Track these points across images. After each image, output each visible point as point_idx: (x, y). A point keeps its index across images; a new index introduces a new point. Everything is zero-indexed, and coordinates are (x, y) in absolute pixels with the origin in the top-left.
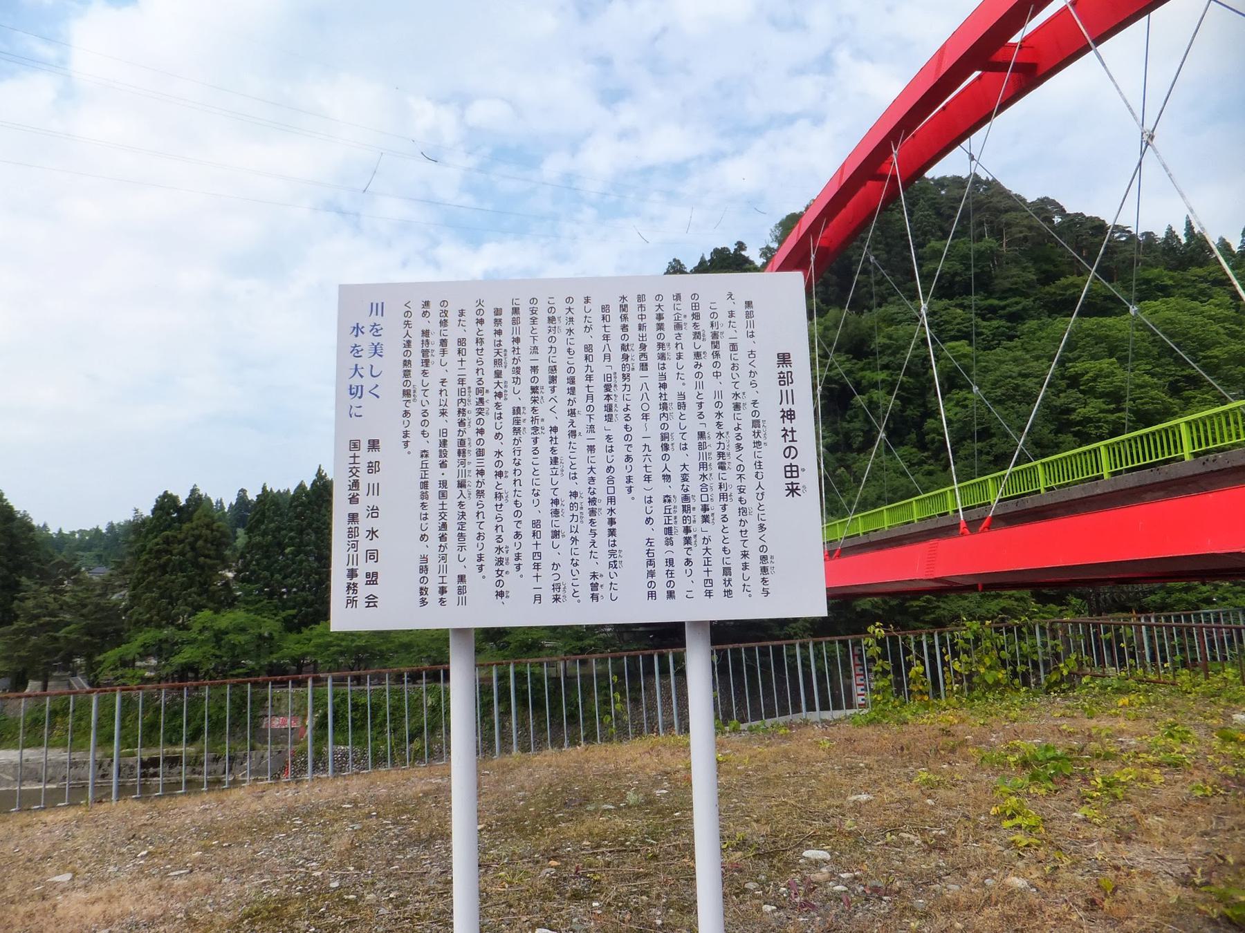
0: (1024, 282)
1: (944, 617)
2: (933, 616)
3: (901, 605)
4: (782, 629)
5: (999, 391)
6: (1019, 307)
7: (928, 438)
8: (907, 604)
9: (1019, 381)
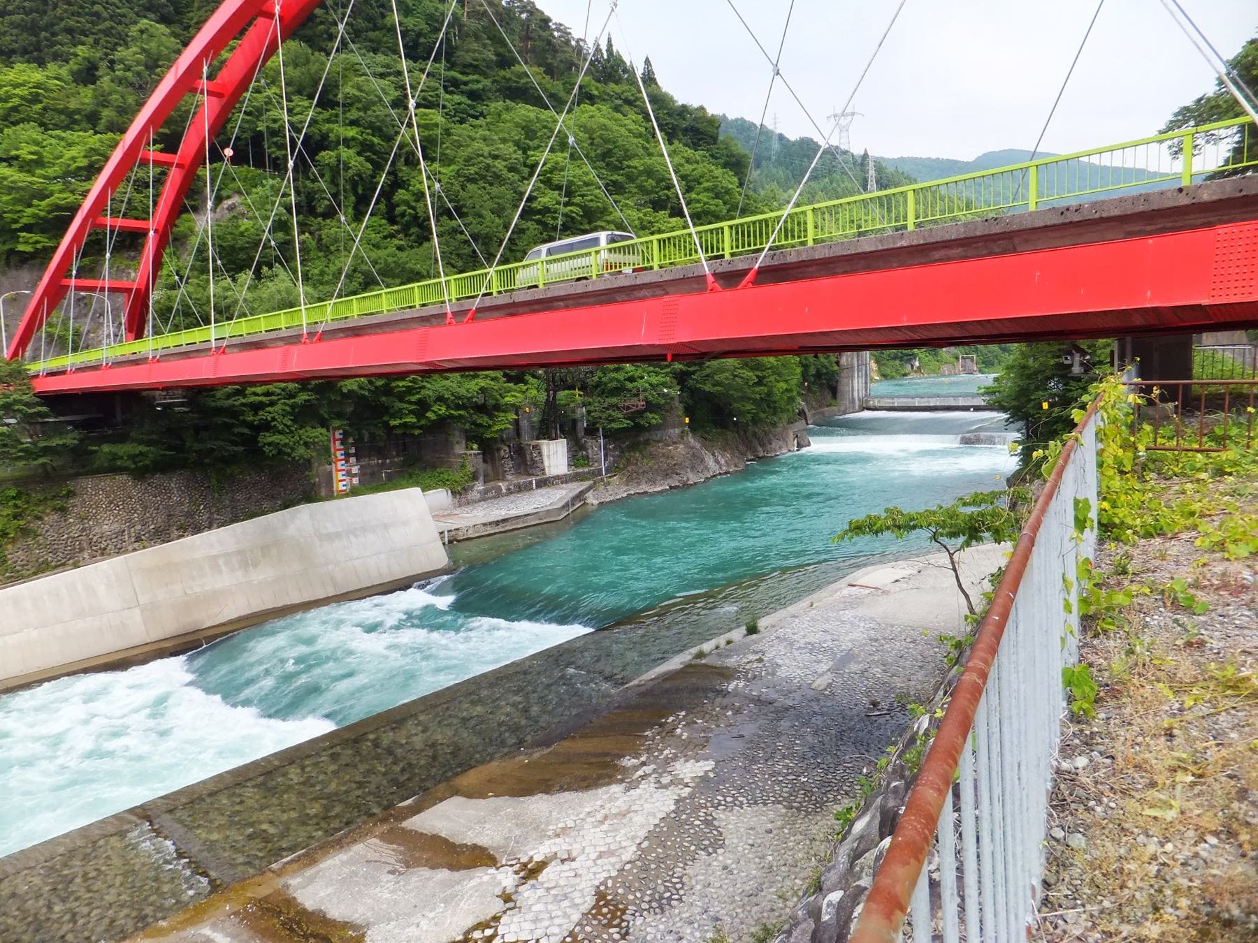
0: (484, 60)
1: (429, 397)
2: (418, 396)
3: (387, 385)
4: (256, 414)
5: (472, 170)
6: (480, 86)
7: (399, 210)
8: (393, 384)
9: (489, 161)
